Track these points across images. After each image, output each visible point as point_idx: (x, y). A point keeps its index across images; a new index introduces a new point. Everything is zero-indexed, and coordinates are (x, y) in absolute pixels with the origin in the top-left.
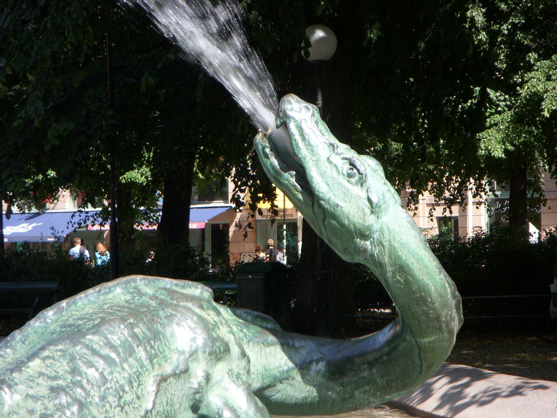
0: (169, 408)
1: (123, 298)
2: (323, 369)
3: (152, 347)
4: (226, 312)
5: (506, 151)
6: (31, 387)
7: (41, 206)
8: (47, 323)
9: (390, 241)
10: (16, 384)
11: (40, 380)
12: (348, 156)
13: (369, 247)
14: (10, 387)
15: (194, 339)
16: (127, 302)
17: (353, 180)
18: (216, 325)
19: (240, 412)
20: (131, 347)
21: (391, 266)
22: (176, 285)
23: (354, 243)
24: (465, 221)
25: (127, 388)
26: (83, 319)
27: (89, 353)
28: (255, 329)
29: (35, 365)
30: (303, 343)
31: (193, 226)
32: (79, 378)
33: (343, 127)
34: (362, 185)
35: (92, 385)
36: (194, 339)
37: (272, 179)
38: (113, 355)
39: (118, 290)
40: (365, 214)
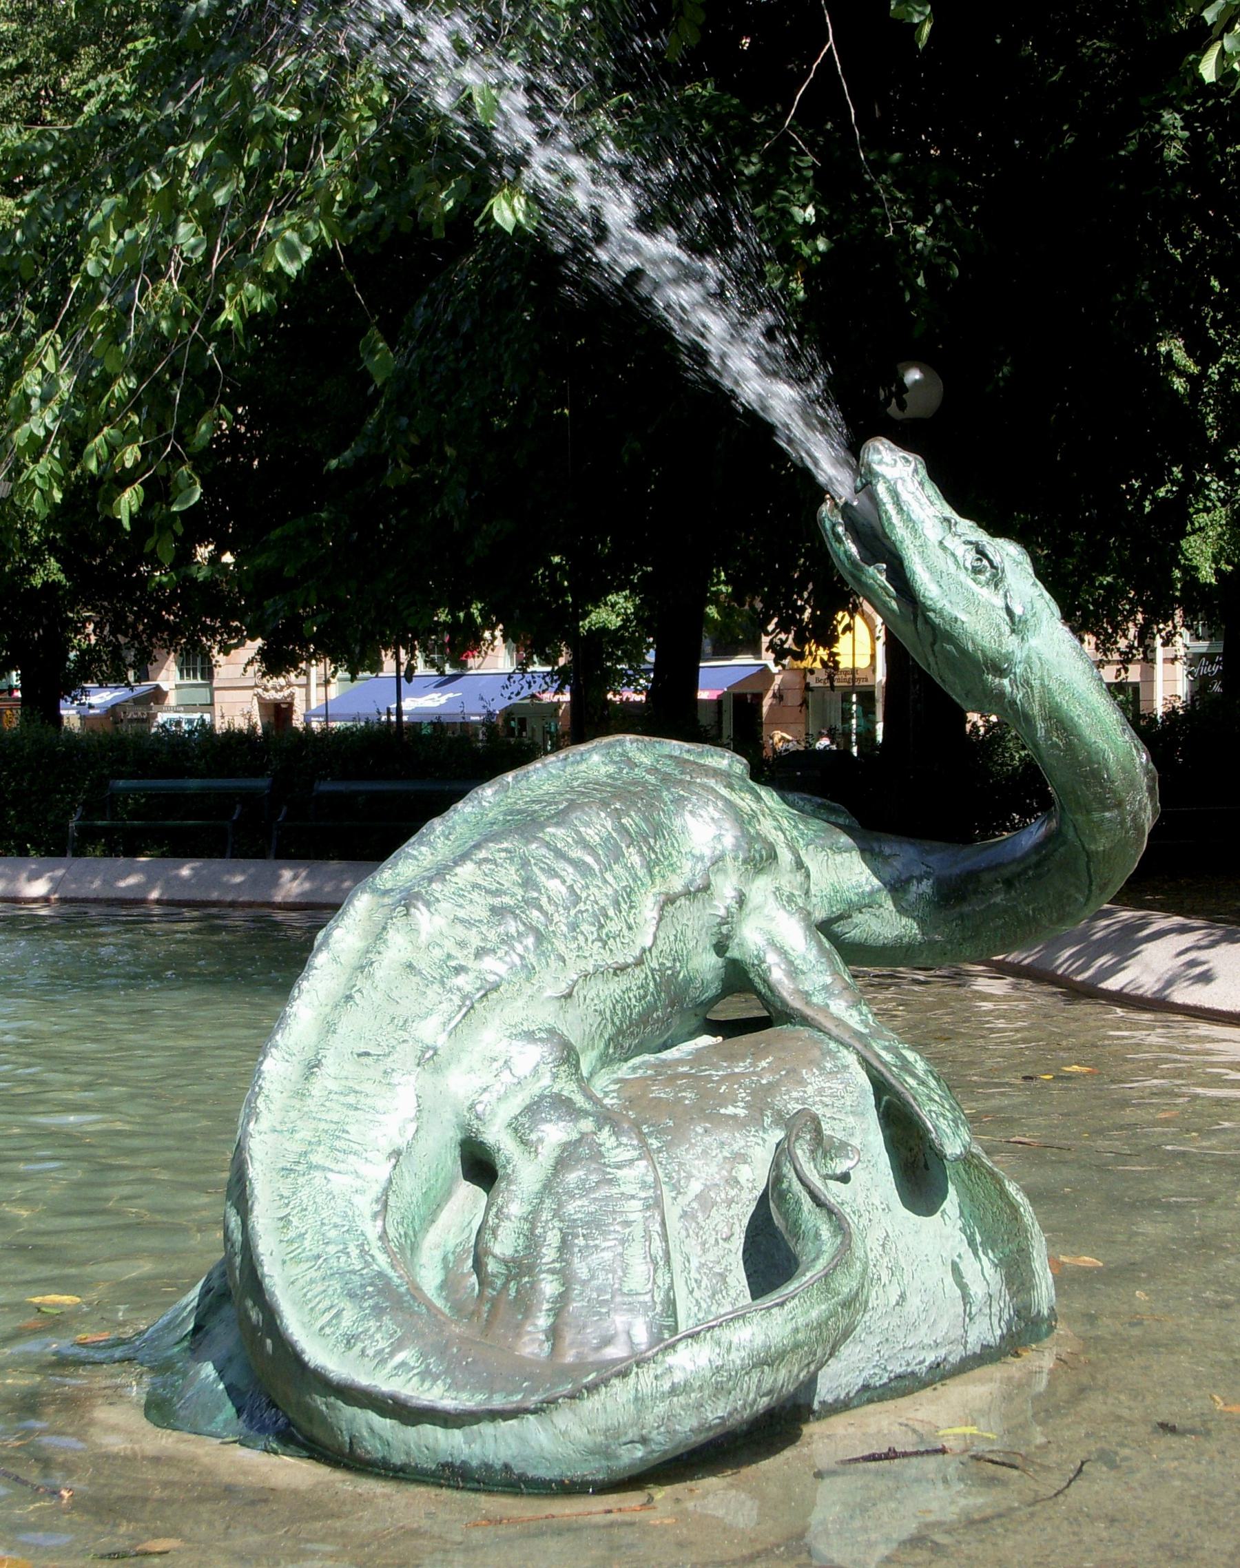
0: (680, 945)
1: (603, 770)
2: (929, 891)
3: (651, 848)
4: (770, 797)
5: (1218, 572)
6: (461, 906)
7: (460, 664)
8: (483, 807)
9: (1042, 679)
10: (438, 900)
11: (475, 896)
12: (973, 539)
13: (1008, 689)
14: (428, 904)
15: (718, 838)
16: (609, 776)
17: (982, 578)
18: (754, 816)
19: (793, 955)
20: (617, 846)
21: (1044, 720)
22: (688, 751)
23: (983, 682)
24: (1151, 690)
25: (611, 912)
26: (540, 802)
27: (550, 855)
28: (817, 824)
29: (466, 871)
30: (896, 849)
31: (703, 695)
32: (535, 895)
33: (966, 489)
34: (996, 586)
35: (557, 905)
36: (718, 838)
37: (848, 578)
38: (589, 860)
39: (596, 758)
40: (1001, 635)
